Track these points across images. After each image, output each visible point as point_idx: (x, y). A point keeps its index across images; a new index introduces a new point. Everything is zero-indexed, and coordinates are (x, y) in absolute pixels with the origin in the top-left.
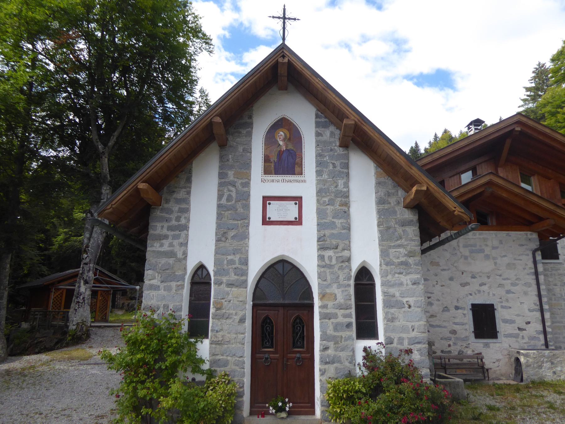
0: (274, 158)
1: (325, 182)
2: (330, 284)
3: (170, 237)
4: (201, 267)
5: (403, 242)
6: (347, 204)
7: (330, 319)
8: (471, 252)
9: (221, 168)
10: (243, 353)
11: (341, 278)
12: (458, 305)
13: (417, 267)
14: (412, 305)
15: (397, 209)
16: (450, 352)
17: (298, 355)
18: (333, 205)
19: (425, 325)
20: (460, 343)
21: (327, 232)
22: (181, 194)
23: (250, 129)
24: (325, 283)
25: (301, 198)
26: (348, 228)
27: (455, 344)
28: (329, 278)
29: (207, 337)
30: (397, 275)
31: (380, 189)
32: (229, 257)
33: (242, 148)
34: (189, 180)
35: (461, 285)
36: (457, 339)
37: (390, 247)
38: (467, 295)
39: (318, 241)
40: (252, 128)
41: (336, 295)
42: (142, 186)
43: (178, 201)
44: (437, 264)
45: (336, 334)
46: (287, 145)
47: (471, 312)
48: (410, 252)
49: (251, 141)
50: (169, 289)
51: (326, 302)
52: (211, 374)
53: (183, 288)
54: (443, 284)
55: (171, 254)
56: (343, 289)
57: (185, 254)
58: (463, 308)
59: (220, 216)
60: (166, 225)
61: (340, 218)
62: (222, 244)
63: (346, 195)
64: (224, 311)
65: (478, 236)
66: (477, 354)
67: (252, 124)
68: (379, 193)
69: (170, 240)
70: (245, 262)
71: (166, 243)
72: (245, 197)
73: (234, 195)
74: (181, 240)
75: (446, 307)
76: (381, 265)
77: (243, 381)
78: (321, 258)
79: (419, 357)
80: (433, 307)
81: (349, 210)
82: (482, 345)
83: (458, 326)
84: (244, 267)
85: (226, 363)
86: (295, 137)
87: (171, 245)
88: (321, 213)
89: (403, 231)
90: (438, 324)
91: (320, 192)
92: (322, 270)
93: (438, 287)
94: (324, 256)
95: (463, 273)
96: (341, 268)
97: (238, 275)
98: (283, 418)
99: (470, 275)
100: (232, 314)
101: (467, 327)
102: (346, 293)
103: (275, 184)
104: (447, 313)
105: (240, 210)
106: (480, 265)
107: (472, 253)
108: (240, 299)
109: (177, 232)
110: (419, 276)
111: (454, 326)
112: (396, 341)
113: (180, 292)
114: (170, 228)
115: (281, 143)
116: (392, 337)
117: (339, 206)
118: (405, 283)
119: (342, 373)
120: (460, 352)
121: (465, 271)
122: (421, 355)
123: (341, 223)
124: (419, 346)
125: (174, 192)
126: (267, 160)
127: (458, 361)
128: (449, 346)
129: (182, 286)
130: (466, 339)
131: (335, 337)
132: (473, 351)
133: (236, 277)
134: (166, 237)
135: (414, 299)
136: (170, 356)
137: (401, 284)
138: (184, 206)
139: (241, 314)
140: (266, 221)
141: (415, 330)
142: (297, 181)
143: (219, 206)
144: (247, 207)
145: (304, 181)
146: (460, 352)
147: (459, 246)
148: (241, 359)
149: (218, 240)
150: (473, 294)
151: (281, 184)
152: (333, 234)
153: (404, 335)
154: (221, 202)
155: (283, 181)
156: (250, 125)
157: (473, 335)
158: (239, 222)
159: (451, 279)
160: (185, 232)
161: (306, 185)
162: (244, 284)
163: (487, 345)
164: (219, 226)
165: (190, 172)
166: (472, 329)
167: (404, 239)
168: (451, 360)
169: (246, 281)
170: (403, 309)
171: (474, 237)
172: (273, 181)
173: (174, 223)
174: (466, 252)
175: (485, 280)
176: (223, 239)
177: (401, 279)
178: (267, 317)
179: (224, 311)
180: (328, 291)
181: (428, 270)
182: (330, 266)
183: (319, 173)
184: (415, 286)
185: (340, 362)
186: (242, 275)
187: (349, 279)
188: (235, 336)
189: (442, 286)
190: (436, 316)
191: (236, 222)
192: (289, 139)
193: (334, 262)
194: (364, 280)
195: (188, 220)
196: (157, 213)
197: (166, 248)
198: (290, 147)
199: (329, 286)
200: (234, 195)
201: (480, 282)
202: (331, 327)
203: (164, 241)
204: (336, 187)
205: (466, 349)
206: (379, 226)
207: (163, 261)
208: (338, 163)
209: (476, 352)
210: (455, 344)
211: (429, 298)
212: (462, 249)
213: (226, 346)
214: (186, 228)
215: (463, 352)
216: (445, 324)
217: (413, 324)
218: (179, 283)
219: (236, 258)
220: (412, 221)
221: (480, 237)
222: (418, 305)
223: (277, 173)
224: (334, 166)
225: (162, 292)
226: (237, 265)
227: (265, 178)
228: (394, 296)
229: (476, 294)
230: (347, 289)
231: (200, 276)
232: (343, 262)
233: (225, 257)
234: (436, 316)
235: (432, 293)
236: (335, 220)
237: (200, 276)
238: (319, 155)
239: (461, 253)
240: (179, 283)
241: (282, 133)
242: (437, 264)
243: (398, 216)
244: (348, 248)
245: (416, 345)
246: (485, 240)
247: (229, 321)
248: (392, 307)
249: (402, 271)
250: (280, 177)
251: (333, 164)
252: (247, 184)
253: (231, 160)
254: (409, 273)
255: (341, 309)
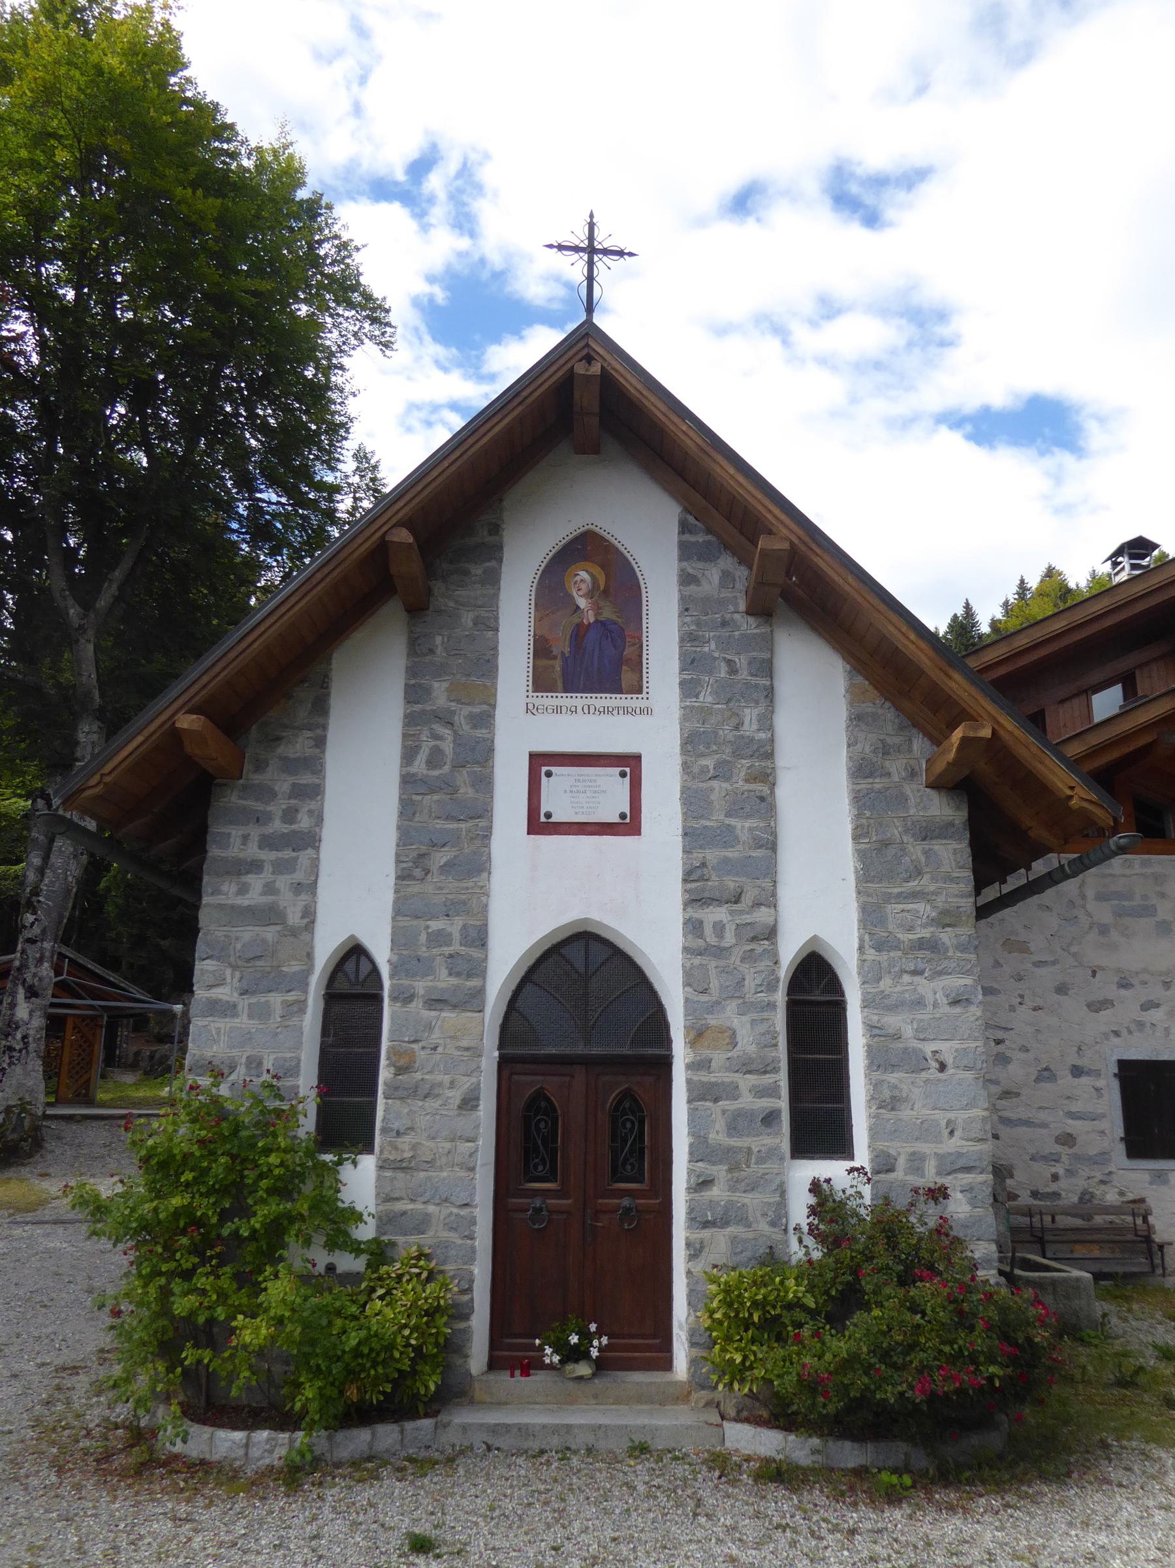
0: (562, 645)
1: (704, 713)
2: (718, 1003)
3: (268, 868)
4: (355, 952)
5: (925, 883)
6: (767, 777)
7: (716, 1100)
8: (1119, 913)
9: (412, 671)
10: (472, 1195)
11: (750, 984)
12: (1079, 1063)
13: (965, 956)
14: (949, 1061)
15: (909, 792)
16: (1056, 1195)
17: (626, 1202)
18: (727, 779)
19: (984, 1119)
20: (1084, 1171)
21: (712, 855)
22: (299, 746)
23: (493, 563)
24: (704, 998)
25: (637, 758)
26: (772, 845)
27: (1070, 1173)
28: (714, 984)
29: (369, 1149)
30: (906, 978)
31: (861, 736)
32: (435, 925)
33: (471, 615)
34: (321, 707)
35: (1089, 1006)
36: (1077, 1158)
37: (888, 898)
38: (1106, 1036)
39: (685, 881)
40: (501, 561)
41: (734, 1033)
42: (186, 722)
43: (291, 766)
44: (1023, 948)
45: (734, 1142)
46: (598, 610)
47: (1115, 1085)
48: (944, 913)
49: (496, 596)
50: (261, 1013)
51: (706, 1053)
52: (379, 1253)
53: (302, 1011)
54: (1039, 1002)
55: (270, 915)
56: (755, 1016)
57: (310, 915)
58: (1097, 1074)
59: (407, 809)
60: (255, 832)
61: (749, 816)
62: (414, 888)
63: (766, 751)
64: (418, 1076)
65: (1137, 869)
66: (1134, 1202)
67: (500, 548)
68: (859, 747)
69: (267, 875)
70: (479, 938)
71: (256, 882)
72: (478, 757)
73: (448, 747)
74: (299, 876)
75: (1046, 1069)
76: (861, 948)
77: (471, 1273)
78: (693, 927)
79: (967, 1208)
80: (1010, 1067)
81: (772, 792)
82: (1147, 1177)
83: (1078, 1123)
84: (475, 953)
85: (421, 1225)
86: (622, 586)
87: (270, 889)
88: (693, 802)
89: (926, 853)
90: (1024, 1117)
91: (691, 743)
92: (697, 961)
93: (1024, 1013)
94: (701, 922)
95: (1094, 974)
96: (749, 957)
97: (458, 974)
98: (581, 1378)
99: (1116, 979)
100: (440, 1084)
101: (1104, 1125)
102: (762, 1028)
103: (565, 719)
104: (1048, 1086)
105: (466, 791)
106: (1141, 951)
107: (1120, 916)
108: (465, 1044)
109: (287, 854)
110: (968, 981)
111: (1070, 1122)
112: (901, 1162)
113: (294, 1021)
114: (267, 842)
115: (582, 603)
116: (893, 1152)
117: (747, 781)
118: (930, 998)
119: (748, 1254)
120: (1086, 1197)
121: (1098, 966)
122: (973, 1202)
123: (751, 829)
124: (967, 1178)
125: (279, 739)
126: (541, 649)
127: (1078, 1222)
128: (1055, 1177)
129: (301, 1006)
130: (1102, 1158)
131: (730, 1150)
132: (1122, 1194)
133: (454, 981)
134: (255, 866)
135: (956, 1044)
136: (263, 1201)
137: (919, 1003)
138: (306, 779)
139: (466, 1083)
140: (539, 824)
141: (957, 1134)
142: (626, 711)
143: (407, 780)
144: (485, 783)
145: (647, 711)
146: (1086, 1197)
147: (1084, 897)
148: (464, 1212)
149: (403, 877)
150: (1124, 1033)
151: (581, 719)
152: (726, 860)
153: (926, 1148)
154: (413, 769)
155: (588, 710)
156: (494, 552)
157: (1121, 1148)
158: (463, 825)
159: (1062, 989)
160: (310, 852)
161: (652, 723)
162: (474, 1000)
163: (1160, 1177)
164: (405, 837)
165: (324, 684)
166: (1120, 1132)
167: (927, 877)
168: (1058, 1218)
169: (481, 992)
170: (924, 1075)
171: (1128, 872)
172: (558, 710)
173: (277, 826)
174: (1103, 913)
175: (1157, 993)
176: (418, 872)
177: (920, 989)
178: (540, 1095)
179: (418, 1076)
180: (712, 1021)
181: (997, 964)
182: (720, 952)
183: (688, 688)
184: (958, 1010)
185: (744, 1221)
186: (469, 976)
187: (772, 987)
188: (448, 1145)
189: (1035, 1009)
190: (1018, 1095)
191: (453, 826)
192: (606, 593)
193: (729, 938)
194: (814, 991)
195: (319, 819)
196: (233, 799)
197: (254, 897)
198: (608, 614)
199: (715, 1007)
200: (448, 747)
201: (1143, 1000)
202: (720, 1124)
203: (250, 879)
204: (737, 728)
205: (1102, 1187)
206: (856, 838)
207: (247, 934)
208: (742, 661)
209: (1130, 1197)
210: (1070, 1173)
211: (998, 1042)
212: (1091, 906)
213: (422, 1174)
214: (311, 840)
215: (1092, 1195)
216: (1043, 1116)
217: (951, 1115)
218: (291, 997)
219: (454, 926)
220: (951, 824)
221: (1144, 871)
222: (965, 1062)
223: (570, 687)
224: (733, 670)
225: (243, 1021)
226: (456, 947)
227: (538, 702)
228: (897, 1037)
229: (1130, 1032)
230: (765, 1015)
231: (352, 977)
232: (754, 939)
233: (421, 923)
234: (1018, 1095)
235: (1006, 1029)
236: (732, 821)
237: (352, 977)
238: (688, 639)
239: (1090, 915)
240: (291, 997)
241: (584, 575)
242: (1023, 948)
243: (912, 812)
244: (770, 900)
245: (960, 1176)
246: (1158, 879)
247: (432, 1104)
248: (894, 1067)
249: (921, 966)
250: (578, 700)
251: (729, 662)
252: (485, 719)
253: (439, 650)
254: (941, 973)
255: (750, 1072)
